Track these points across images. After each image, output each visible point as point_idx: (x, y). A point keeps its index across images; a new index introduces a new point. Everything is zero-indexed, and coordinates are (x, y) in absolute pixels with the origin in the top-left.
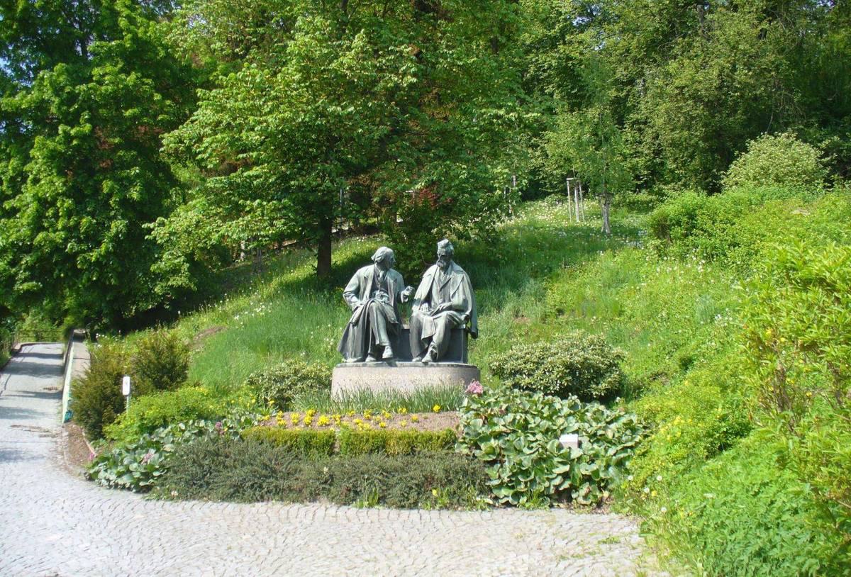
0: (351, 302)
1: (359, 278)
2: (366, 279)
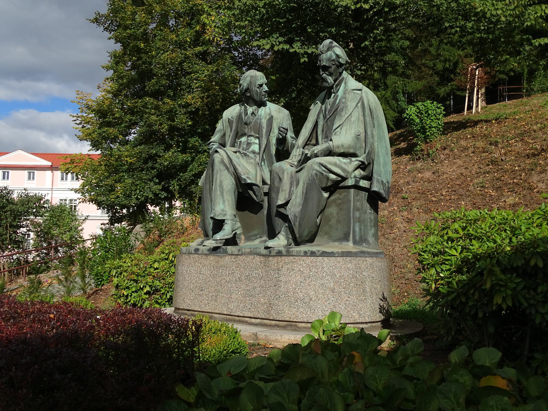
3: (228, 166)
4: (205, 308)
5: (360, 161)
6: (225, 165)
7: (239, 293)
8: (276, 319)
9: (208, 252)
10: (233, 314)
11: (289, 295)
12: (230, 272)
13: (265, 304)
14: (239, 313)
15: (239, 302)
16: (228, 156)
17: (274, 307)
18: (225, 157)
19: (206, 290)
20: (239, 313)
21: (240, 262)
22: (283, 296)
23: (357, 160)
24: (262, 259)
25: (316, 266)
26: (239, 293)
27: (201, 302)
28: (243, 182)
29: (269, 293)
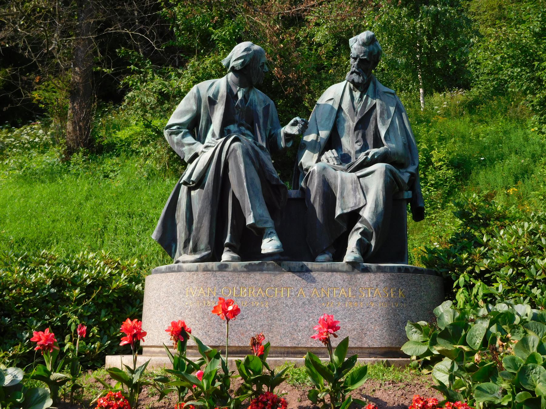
0: (183, 145)
1: (199, 100)
3: (254, 160)
5: (410, 173)
6: (251, 158)
7: (311, 319)
8: (373, 346)
9: (245, 269)
10: (302, 346)
12: (293, 294)
13: (354, 330)
14: (312, 344)
17: (368, 333)
19: (250, 319)
20: (312, 344)
22: (381, 319)
23: (407, 172)
24: (345, 276)
25: (415, 284)
26: (311, 319)
28: (274, 183)
29: (360, 317)
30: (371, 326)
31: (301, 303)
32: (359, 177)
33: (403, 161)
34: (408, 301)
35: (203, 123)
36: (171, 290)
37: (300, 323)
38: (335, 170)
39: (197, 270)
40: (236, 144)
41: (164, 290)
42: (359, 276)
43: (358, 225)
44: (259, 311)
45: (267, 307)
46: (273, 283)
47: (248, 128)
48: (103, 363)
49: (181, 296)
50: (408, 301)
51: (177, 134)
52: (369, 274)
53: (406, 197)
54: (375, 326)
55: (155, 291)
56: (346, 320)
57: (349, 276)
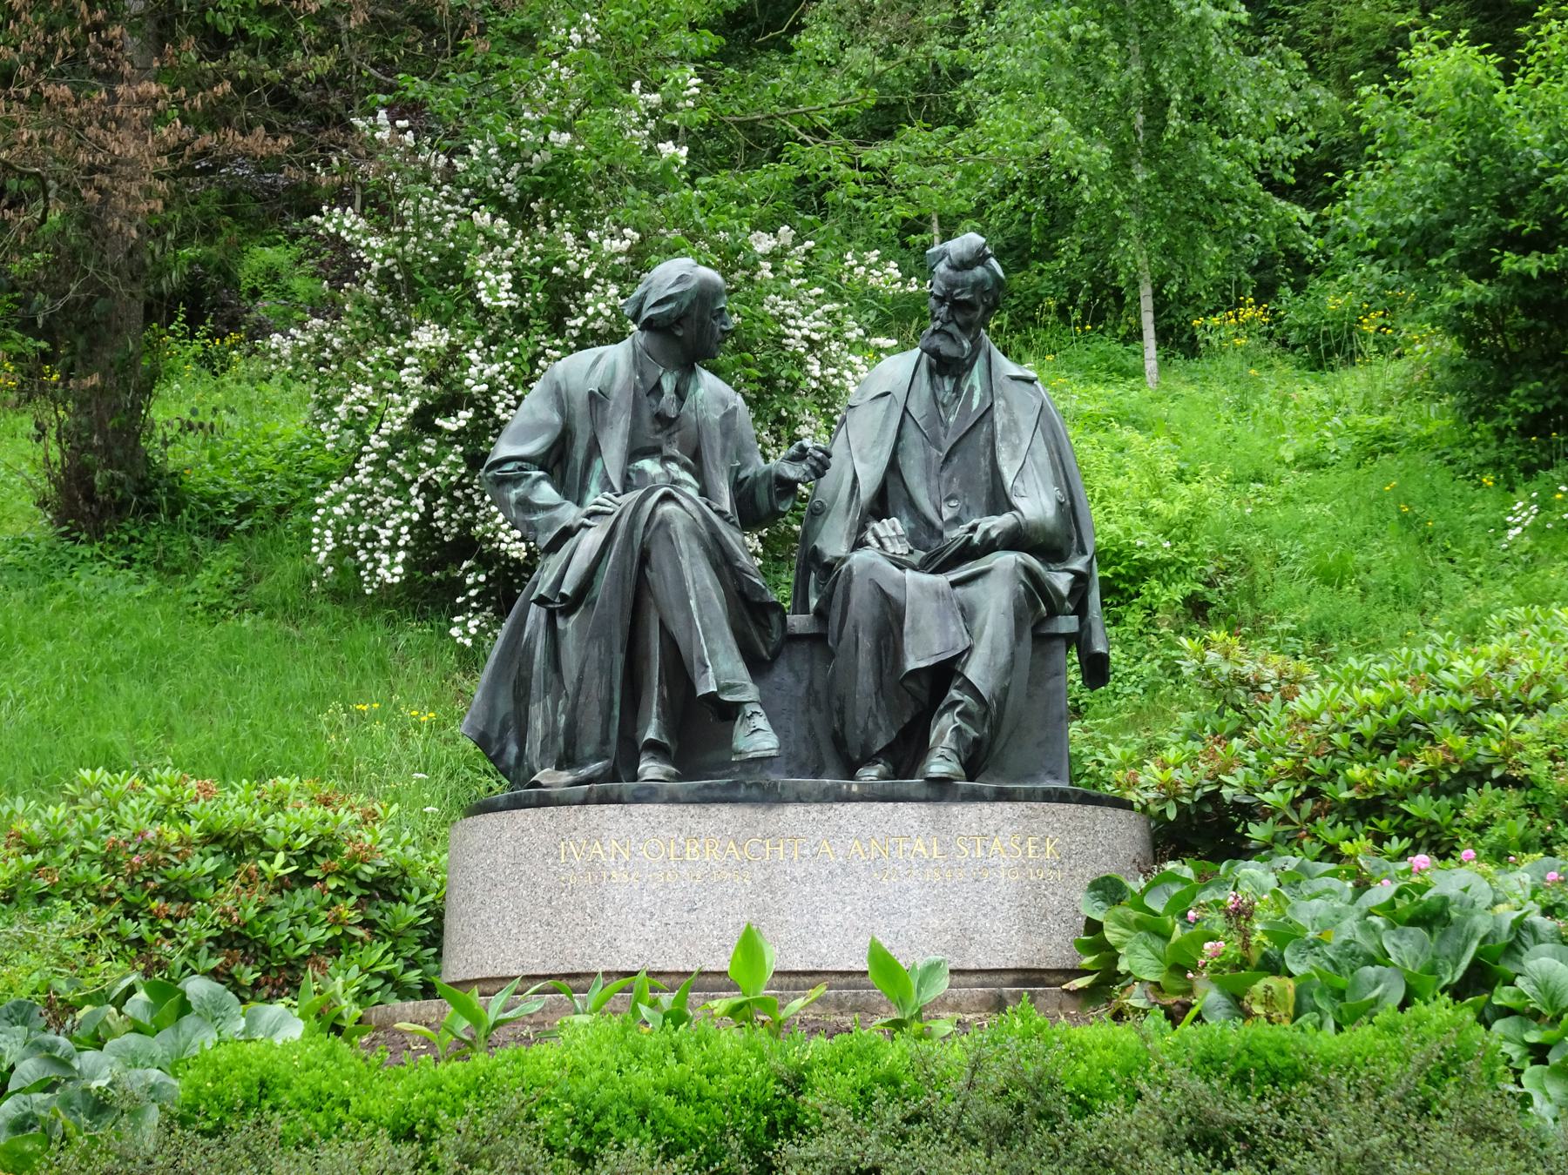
1: (561, 399)
2: (597, 400)
4: (712, 962)
5: (1072, 572)
7: (849, 908)
11: (1024, 901)
12: (806, 852)
13: (946, 931)
15: (851, 934)
16: (706, 518)
17: (977, 936)
18: (698, 516)
19: (710, 909)
21: (842, 822)
22: (1007, 905)
26: (849, 908)
27: (693, 944)
29: (958, 901)
30: (983, 921)
31: (824, 873)
32: (954, 584)
33: (1058, 542)
34: (1067, 866)
35: (579, 453)
36: (523, 850)
37: (823, 918)
38: (900, 568)
39: (585, 802)
40: (669, 507)
41: (508, 849)
42: (956, 809)
43: (954, 694)
44: (731, 891)
45: (749, 883)
46: (761, 827)
47: (685, 467)
48: (1100, 654)
49: (550, 861)
50: (1067, 866)
51: (516, 481)
52: (980, 805)
53: (1063, 630)
54: (993, 921)
55: (483, 855)
56: (928, 910)
57: (933, 811)
